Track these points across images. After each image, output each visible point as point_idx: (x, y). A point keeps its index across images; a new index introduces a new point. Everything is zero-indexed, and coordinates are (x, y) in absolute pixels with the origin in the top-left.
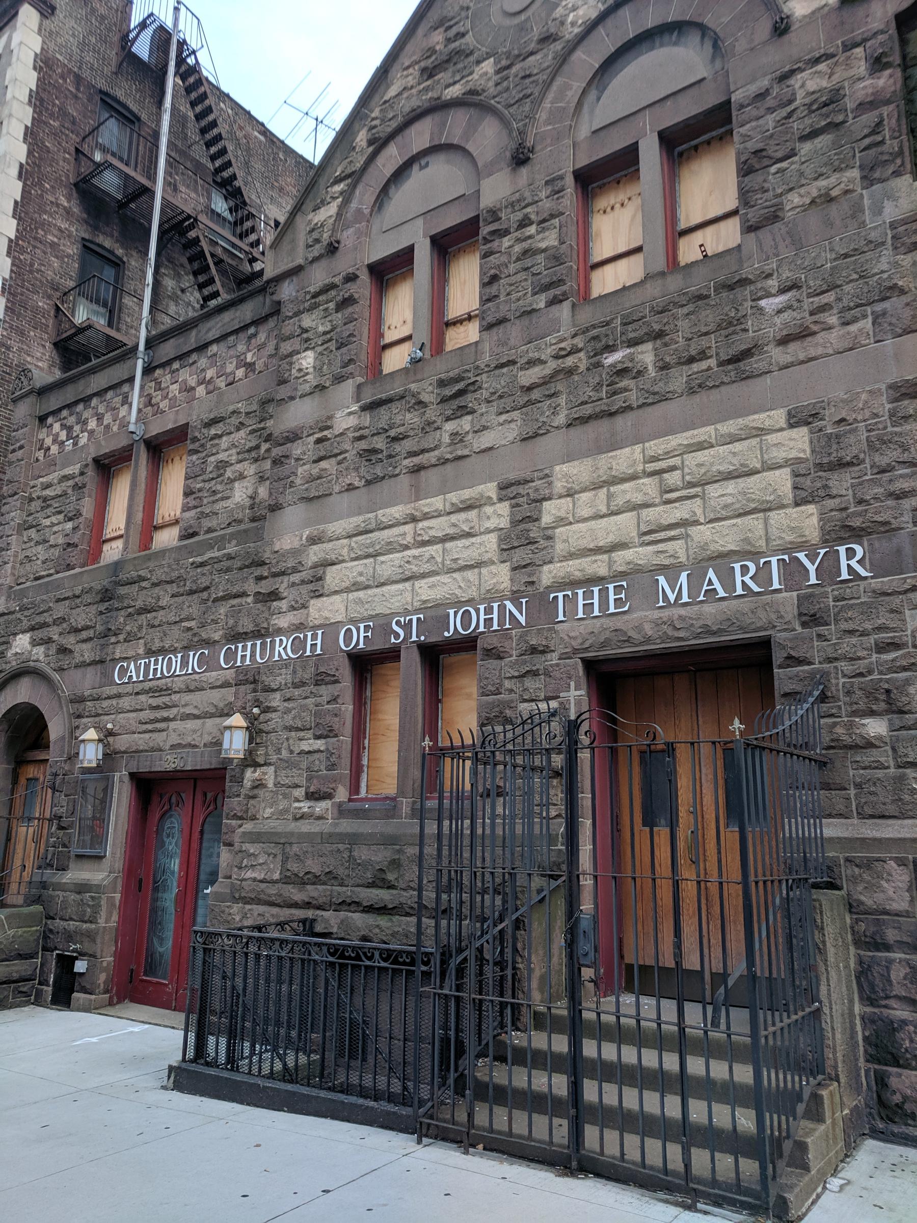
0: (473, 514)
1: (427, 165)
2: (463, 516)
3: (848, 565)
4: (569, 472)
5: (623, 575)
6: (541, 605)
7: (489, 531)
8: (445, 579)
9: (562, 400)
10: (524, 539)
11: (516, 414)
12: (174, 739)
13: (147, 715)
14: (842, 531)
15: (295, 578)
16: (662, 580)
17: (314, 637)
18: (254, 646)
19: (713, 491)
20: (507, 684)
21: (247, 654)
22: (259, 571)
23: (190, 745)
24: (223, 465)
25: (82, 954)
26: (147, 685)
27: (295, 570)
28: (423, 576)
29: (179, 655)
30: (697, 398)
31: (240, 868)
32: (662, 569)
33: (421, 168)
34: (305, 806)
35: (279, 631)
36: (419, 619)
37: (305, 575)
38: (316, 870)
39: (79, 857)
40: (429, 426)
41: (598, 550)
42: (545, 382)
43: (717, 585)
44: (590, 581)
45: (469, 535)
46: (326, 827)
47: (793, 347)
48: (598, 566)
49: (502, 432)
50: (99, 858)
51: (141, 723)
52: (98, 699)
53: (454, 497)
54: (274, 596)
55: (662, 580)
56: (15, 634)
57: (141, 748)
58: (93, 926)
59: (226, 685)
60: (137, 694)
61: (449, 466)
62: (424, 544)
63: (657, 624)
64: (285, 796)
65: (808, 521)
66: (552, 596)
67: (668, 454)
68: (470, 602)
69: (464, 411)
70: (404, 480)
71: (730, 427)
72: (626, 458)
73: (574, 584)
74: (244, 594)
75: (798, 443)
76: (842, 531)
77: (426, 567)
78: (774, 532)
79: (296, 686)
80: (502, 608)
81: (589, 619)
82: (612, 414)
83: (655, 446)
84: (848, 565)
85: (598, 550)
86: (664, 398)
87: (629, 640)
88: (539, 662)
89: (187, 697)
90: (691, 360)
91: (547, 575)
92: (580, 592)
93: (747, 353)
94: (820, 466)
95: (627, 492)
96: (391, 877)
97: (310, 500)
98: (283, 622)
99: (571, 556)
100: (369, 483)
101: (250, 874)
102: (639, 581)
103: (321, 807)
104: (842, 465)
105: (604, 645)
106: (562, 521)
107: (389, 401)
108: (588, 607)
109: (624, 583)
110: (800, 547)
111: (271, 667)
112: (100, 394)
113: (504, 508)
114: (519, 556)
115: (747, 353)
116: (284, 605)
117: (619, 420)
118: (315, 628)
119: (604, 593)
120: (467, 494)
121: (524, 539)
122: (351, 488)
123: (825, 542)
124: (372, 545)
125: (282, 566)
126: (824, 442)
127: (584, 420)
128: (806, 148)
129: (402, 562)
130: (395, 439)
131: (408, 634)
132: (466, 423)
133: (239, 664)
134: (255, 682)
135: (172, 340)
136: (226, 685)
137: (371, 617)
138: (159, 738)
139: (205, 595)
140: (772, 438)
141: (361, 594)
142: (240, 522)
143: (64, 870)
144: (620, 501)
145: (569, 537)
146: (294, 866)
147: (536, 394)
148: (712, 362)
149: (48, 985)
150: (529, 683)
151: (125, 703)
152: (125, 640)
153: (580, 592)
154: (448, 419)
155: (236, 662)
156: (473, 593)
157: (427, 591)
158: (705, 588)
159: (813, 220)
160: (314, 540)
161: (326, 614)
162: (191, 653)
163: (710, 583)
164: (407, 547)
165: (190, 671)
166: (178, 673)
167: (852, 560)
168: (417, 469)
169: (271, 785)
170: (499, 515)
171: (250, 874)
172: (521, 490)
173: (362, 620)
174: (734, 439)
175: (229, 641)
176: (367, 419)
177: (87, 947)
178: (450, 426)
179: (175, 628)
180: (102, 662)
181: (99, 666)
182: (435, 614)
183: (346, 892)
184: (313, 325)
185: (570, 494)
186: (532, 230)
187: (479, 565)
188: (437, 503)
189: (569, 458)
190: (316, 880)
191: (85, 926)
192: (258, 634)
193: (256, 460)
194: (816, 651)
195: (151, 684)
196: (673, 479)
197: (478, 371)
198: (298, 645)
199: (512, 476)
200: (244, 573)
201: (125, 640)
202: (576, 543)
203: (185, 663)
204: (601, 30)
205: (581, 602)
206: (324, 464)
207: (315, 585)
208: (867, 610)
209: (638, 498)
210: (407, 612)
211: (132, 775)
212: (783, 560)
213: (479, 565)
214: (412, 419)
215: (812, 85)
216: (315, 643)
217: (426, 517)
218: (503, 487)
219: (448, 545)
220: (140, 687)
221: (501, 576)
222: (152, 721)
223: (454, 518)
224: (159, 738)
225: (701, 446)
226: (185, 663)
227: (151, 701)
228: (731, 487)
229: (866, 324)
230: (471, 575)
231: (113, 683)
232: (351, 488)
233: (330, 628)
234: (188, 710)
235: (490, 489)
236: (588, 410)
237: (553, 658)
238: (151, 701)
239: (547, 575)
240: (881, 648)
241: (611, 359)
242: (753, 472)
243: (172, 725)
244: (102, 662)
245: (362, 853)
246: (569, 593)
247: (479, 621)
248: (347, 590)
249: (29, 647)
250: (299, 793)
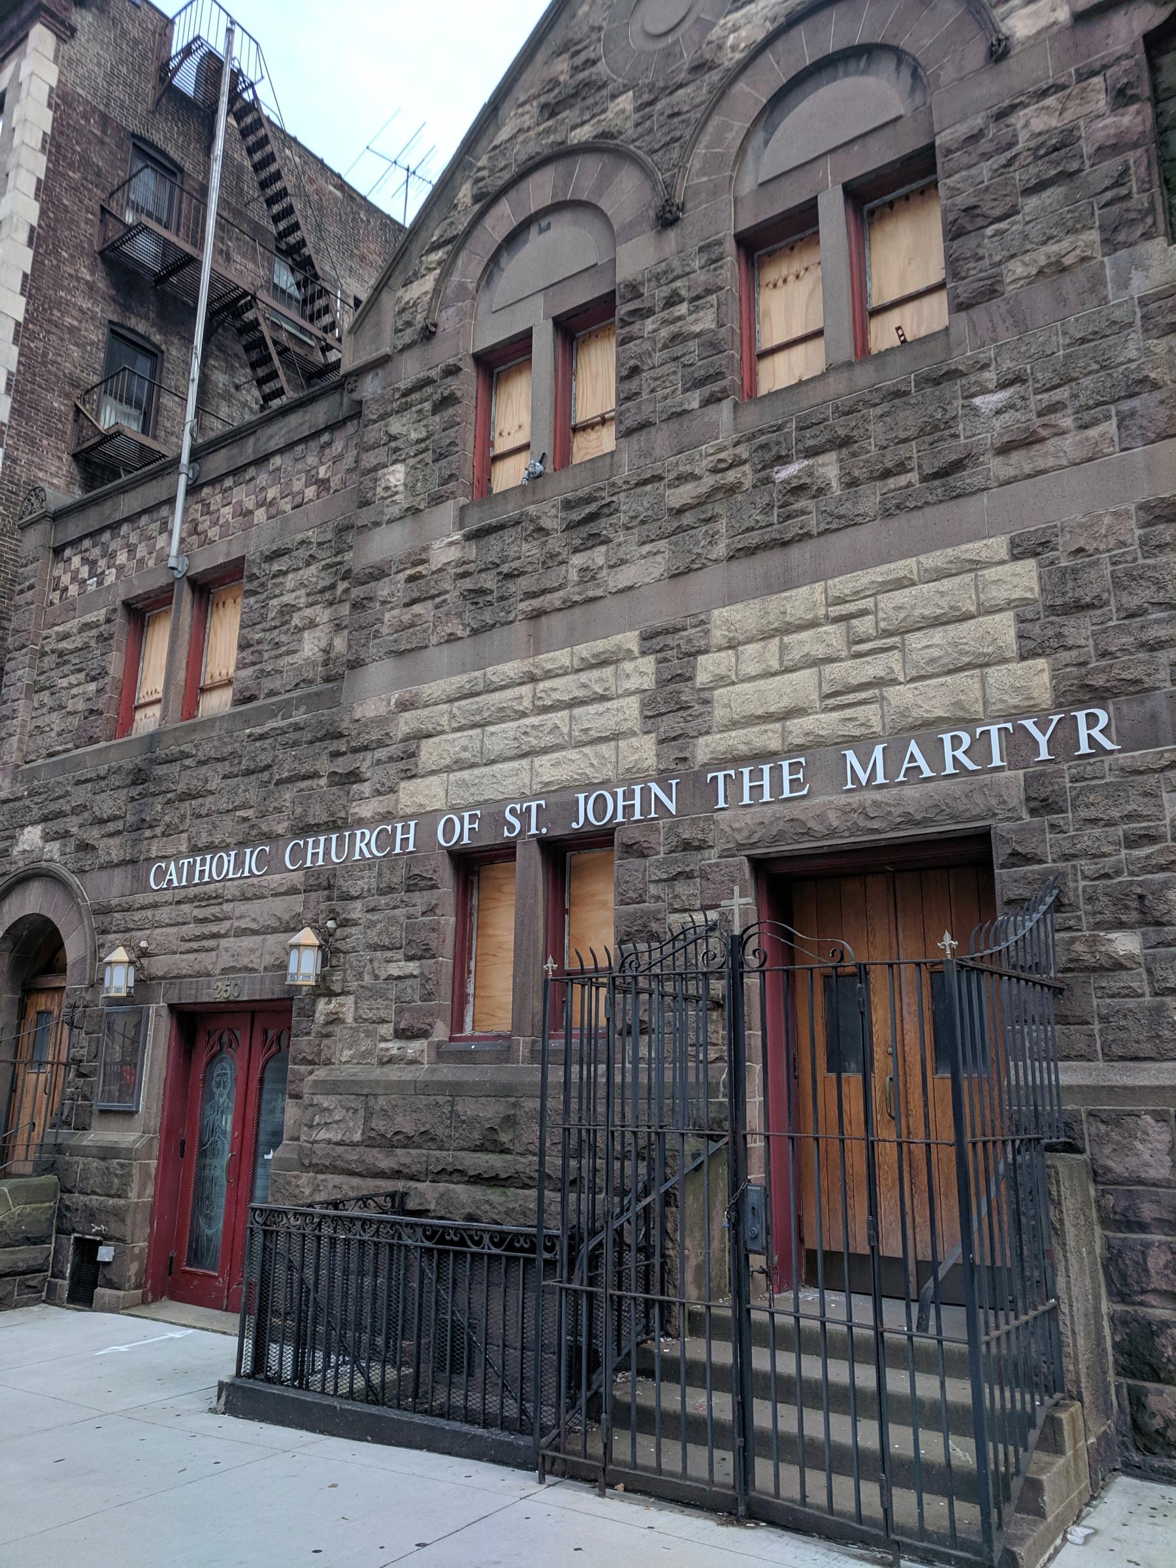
0: (608, 671)
1: (549, 226)
2: (595, 674)
3: (1089, 736)
4: (729, 618)
5: (801, 749)
6: (696, 786)
7: (629, 693)
8: (572, 754)
9: (722, 526)
10: (674, 704)
11: (663, 544)
12: (226, 961)
13: (191, 930)
14: (1082, 692)
15: (381, 754)
16: (851, 756)
17: (406, 829)
18: (328, 841)
19: (916, 641)
20: (653, 890)
21: (319, 851)
22: (335, 745)
23: (247, 969)
24: (288, 610)
25: (107, 1238)
26: (192, 892)
27: (381, 744)
28: (545, 751)
29: (233, 853)
30: (894, 523)
31: (311, 1127)
32: (850, 741)
33: (541, 231)
34: (394, 1047)
35: (360, 822)
36: (539, 806)
37: (392, 750)
38: (409, 1129)
39: (104, 1112)
40: (552, 560)
41: (768, 718)
42: (701, 502)
43: (921, 762)
44: (757, 757)
45: (603, 698)
46: (420, 1074)
47: (1016, 456)
48: (769, 738)
49: (645, 568)
50: (131, 1114)
51: (183, 940)
52: (128, 910)
53: (584, 650)
54: (354, 776)
55: (851, 756)
56: (23, 827)
57: (184, 972)
58: (122, 1202)
59: (293, 891)
60: (179, 902)
61: (577, 612)
62: (546, 710)
63: (845, 811)
64: (368, 1034)
65: (1038, 678)
66: (710, 776)
67: (858, 595)
68: (604, 784)
69: (597, 540)
70: (521, 629)
71: (935, 559)
72: (803, 600)
73: (738, 760)
74: (315, 775)
75: (1023, 579)
76: (1082, 692)
77: (549, 740)
78: (994, 694)
79: (382, 892)
80: (646, 791)
81: (759, 805)
82: (785, 544)
83: (841, 585)
84: (1089, 736)
85: (768, 718)
86: (852, 523)
87: (808, 833)
88: (694, 862)
89: (242, 908)
90: (887, 474)
91: (704, 749)
92: (746, 771)
93: (957, 466)
94: (1052, 609)
95: (805, 643)
96: (504, 1138)
97: (400, 654)
98: (365, 810)
99: (734, 725)
100: (475, 632)
101: (323, 1135)
102: (818, 756)
103: (414, 1048)
104: (1079, 607)
105: (775, 839)
106: (722, 681)
107: (501, 527)
108: (757, 790)
109: (802, 760)
110: (1026, 713)
111: (350, 868)
112: (132, 519)
113: (648, 664)
114: (668, 725)
115: (957, 466)
116: (366, 788)
117: (795, 552)
118: (406, 818)
119: (776, 771)
120: (600, 645)
121: (674, 704)
122: (452, 639)
123: (1058, 706)
124: (480, 711)
125: (364, 739)
126: (1056, 578)
127: (751, 551)
128: (1031, 204)
129: (516, 733)
130: (509, 576)
131: (526, 825)
132: (598, 556)
133: (309, 864)
134: (329, 887)
135: (223, 451)
136: (293, 891)
137: (478, 805)
138: (207, 960)
139: (265, 776)
140: (990, 573)
141: (465, 774)
142: (311, 682)
143: (84, 1129)
144: (796, 655)
145: (733, 700)
146: (379, 1125)
147: (688, 519)
148: (914, 477)
149: (64, 1278)
150: (681, 888)
151: (164, 914)
152: (163, 834)
153: (746, 771)
154: (576, 551)
155: (393, 849)
156: (608, 772)
157: (548, 770)
158: (906, 765)
159: (1041, 296)
160: (405, 706)
161: (420, 800)
162: (248, 851)
163: (912, 758)
164: (523, 715)
165: (246, 874)
166: (231, 876)
167: (1093, 729)
168: (537, 615)
169: (349, 1019)
170: (642, 673)
171: (323, 1135)
172: (670, 640)
173: (467, 808)
174: (941, 575)
175: (296, 835)
176: (472, 551)
177: (114, 1229)
178: (578, 560)
179: (228, 818)
180: (133, 862)
181: (130, 867)
182: (560, 799)
183: (447, 1158)
184: (404, 430)
185: (732, 645)
186: (682, 309)
187: (616, 737)
188: (562, 657)
189: (730, 599)
190: (408, 1142)
191: (111, 1201)
192: (333, 826)
193: (331, 604)
194: (1049, 845)
195: (196, 890)
196: (864, 626)
197: (615, 490)
198: (385, 839)
199: (658, 623)
200: (315, 748)
201: (163, 834)
202: (741, 709)
203: (239, 863)
204: (769, 55)
205: (747, 784)
206: (417, 608)
207: (407, 762)
208: (1115, 792)
209: (820, 651)
210: (524, 798)
211: (172, 1007)
212: (1006, 729)
213: (616, 737)
214: (531, 550)
215: (1038, 125)
216: (406, 837)
217: (549, 675)
218: (646, 637)
219: (577, 711)
220: (183, 893)
221: (643, 751)
222: (198, 938)
223: (584, 677)
224: (207, 960)
225: (899, 584)
226: (239, 863)
227: (196, 912)
228: (938, 636)
229: (1111, 427)
230: (606, 749)
231: (147, 888)
232: (452, 639)
233: (426, 818)
234: (244, 924)
235: (630, 640)
236: (754, 538)
237: (712, 856)
238: (196, 912)
239: (704, 749)
240: (1133, 842)
241: (784, 473)
242: (967, 617)
243: (224, 943)
244: (133, 862)
245: (468, 1108)
246: (732, 772)
247: (615, 808)
248: (448, 769)
249: (40, 843)
250: (386, 1030)
